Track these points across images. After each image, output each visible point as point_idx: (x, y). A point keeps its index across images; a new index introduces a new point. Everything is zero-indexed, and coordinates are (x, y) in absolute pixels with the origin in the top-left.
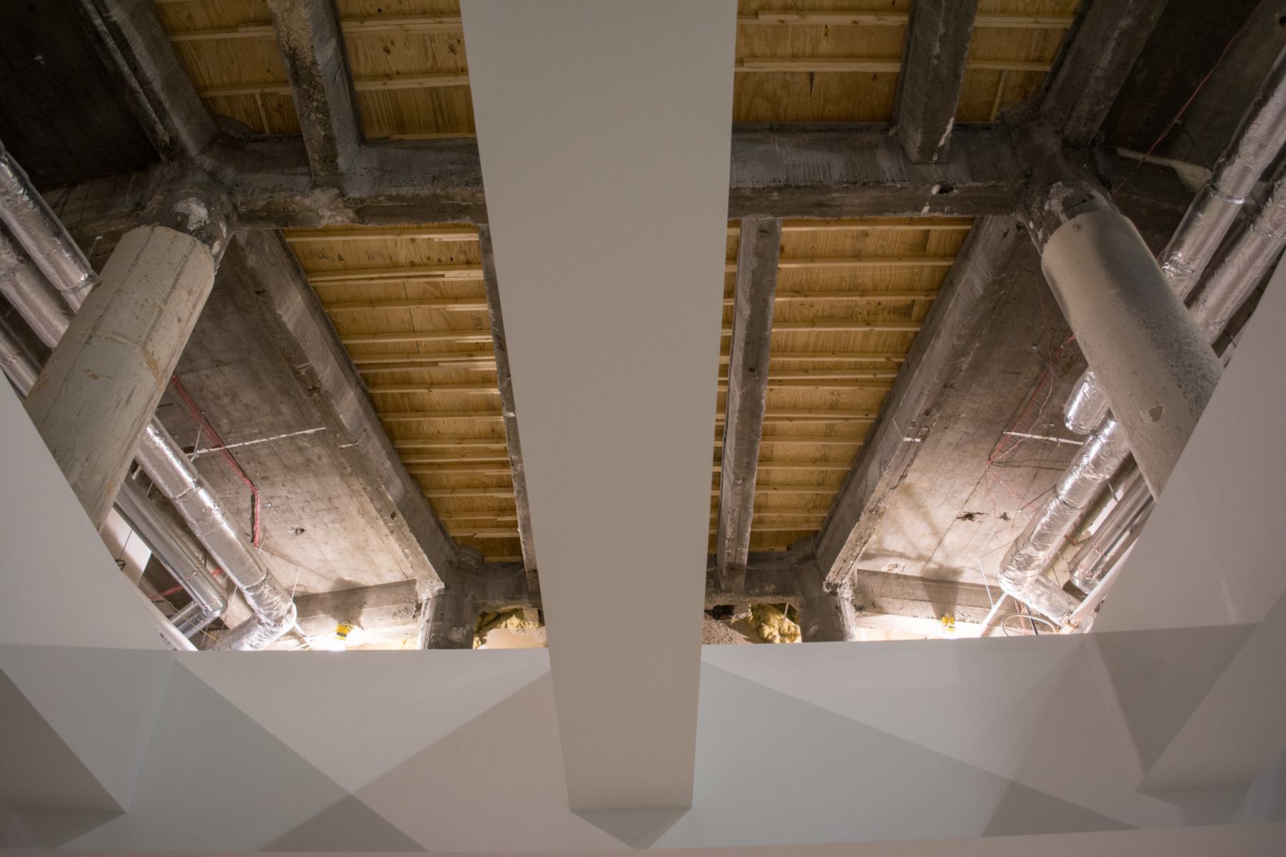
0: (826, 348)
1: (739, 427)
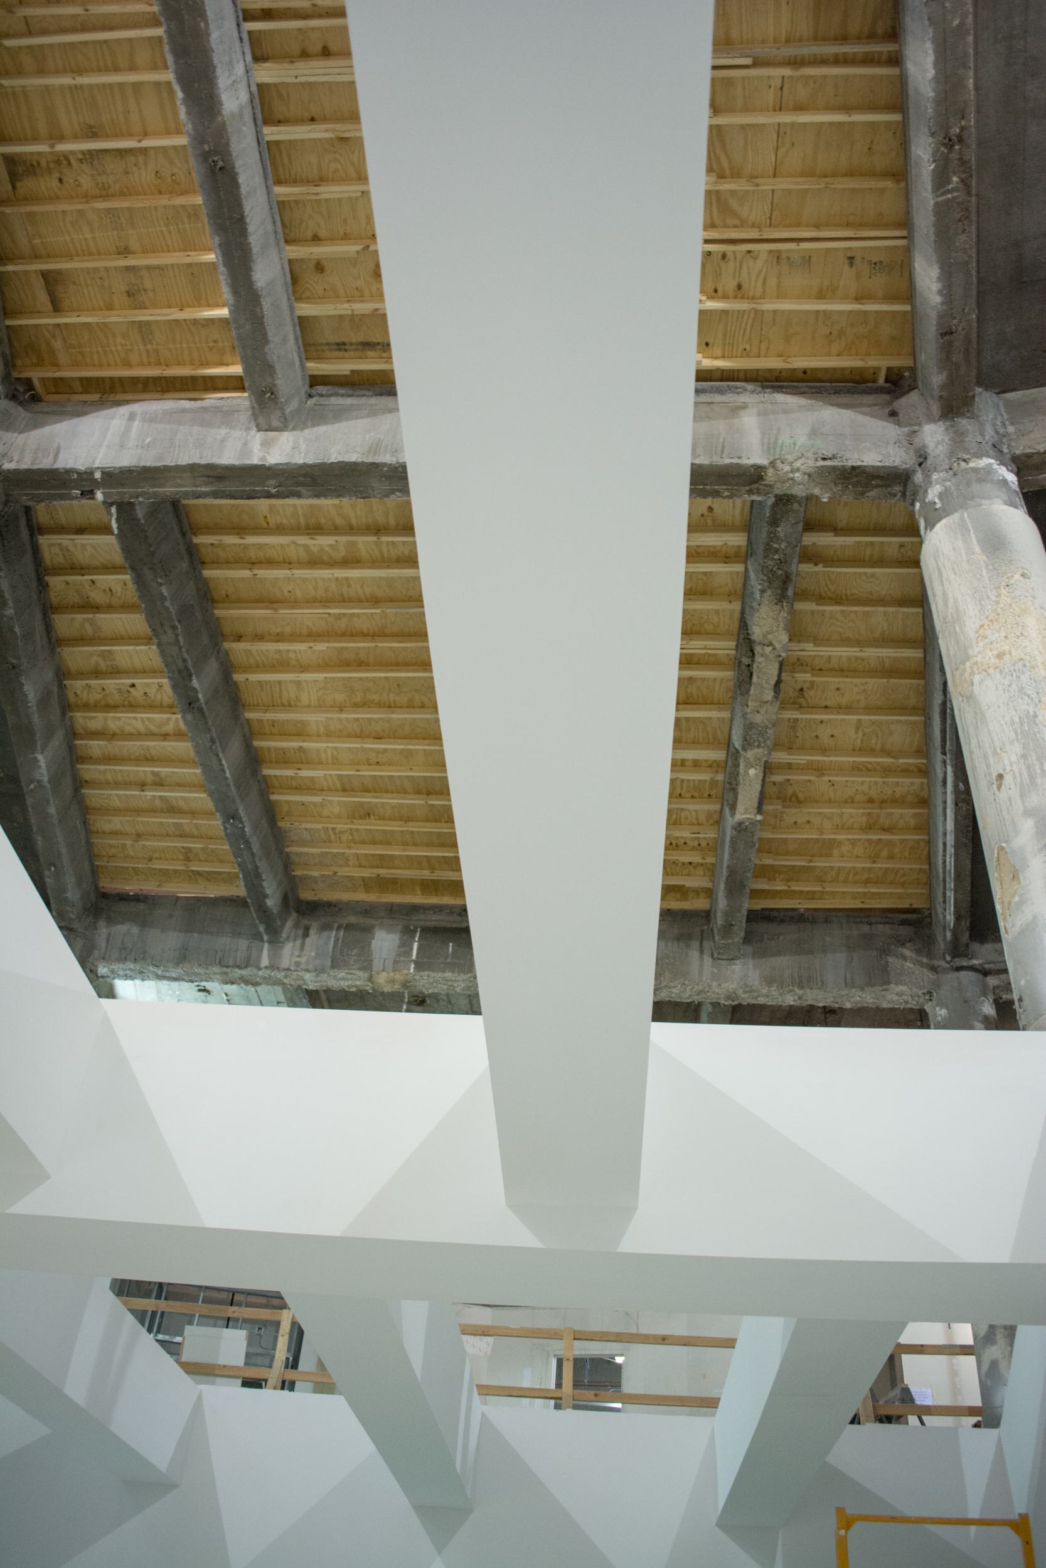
1: (202, 25)
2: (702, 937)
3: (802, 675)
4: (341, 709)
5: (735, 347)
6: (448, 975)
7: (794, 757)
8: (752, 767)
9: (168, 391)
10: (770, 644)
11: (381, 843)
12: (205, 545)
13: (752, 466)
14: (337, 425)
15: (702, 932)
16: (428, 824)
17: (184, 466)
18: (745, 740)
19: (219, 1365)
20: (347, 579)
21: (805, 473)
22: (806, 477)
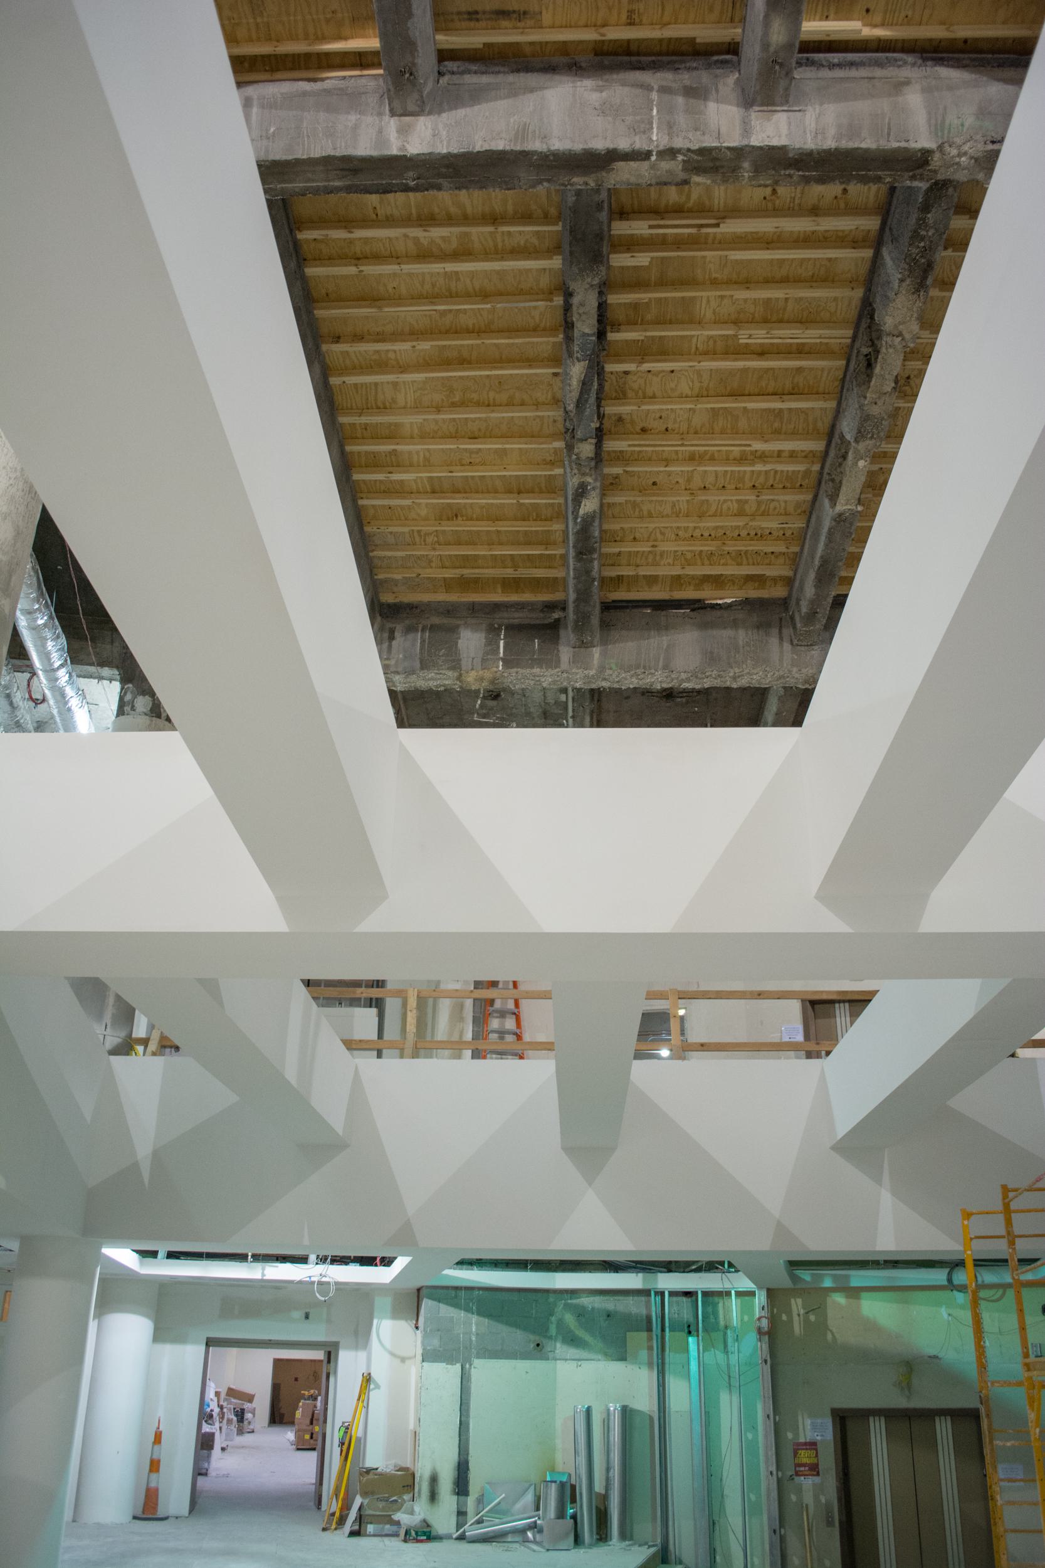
0: (374, 463)
2: (780, 623)
3: (913, 363)
4: (438, 409)
5: (896, 15)
6: (536, 670)
7: (890, 446)
8: (862, 459)
9: (278, 70)
10: (900, 335)
11: (467, 544)
12: (307, 240)
13: (920, 150)
14: (476, 108)
15: (781, 619)
16: (515, 523)
17: (317, 159)
18: (859, 432)
19: (355, 1041)
20: (457, 273)
21: (971, 158)
22: (973, 161)
